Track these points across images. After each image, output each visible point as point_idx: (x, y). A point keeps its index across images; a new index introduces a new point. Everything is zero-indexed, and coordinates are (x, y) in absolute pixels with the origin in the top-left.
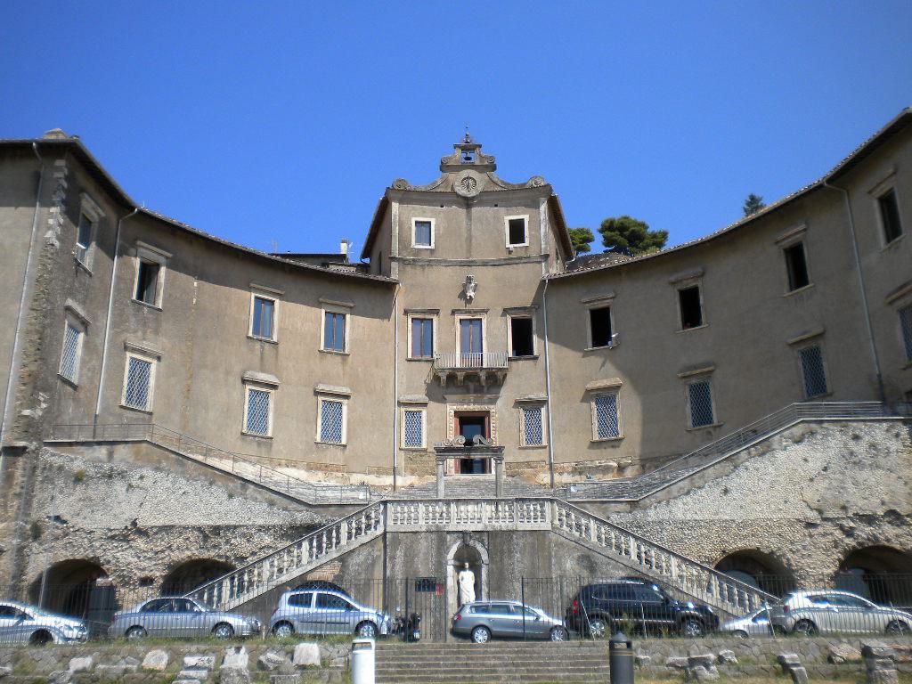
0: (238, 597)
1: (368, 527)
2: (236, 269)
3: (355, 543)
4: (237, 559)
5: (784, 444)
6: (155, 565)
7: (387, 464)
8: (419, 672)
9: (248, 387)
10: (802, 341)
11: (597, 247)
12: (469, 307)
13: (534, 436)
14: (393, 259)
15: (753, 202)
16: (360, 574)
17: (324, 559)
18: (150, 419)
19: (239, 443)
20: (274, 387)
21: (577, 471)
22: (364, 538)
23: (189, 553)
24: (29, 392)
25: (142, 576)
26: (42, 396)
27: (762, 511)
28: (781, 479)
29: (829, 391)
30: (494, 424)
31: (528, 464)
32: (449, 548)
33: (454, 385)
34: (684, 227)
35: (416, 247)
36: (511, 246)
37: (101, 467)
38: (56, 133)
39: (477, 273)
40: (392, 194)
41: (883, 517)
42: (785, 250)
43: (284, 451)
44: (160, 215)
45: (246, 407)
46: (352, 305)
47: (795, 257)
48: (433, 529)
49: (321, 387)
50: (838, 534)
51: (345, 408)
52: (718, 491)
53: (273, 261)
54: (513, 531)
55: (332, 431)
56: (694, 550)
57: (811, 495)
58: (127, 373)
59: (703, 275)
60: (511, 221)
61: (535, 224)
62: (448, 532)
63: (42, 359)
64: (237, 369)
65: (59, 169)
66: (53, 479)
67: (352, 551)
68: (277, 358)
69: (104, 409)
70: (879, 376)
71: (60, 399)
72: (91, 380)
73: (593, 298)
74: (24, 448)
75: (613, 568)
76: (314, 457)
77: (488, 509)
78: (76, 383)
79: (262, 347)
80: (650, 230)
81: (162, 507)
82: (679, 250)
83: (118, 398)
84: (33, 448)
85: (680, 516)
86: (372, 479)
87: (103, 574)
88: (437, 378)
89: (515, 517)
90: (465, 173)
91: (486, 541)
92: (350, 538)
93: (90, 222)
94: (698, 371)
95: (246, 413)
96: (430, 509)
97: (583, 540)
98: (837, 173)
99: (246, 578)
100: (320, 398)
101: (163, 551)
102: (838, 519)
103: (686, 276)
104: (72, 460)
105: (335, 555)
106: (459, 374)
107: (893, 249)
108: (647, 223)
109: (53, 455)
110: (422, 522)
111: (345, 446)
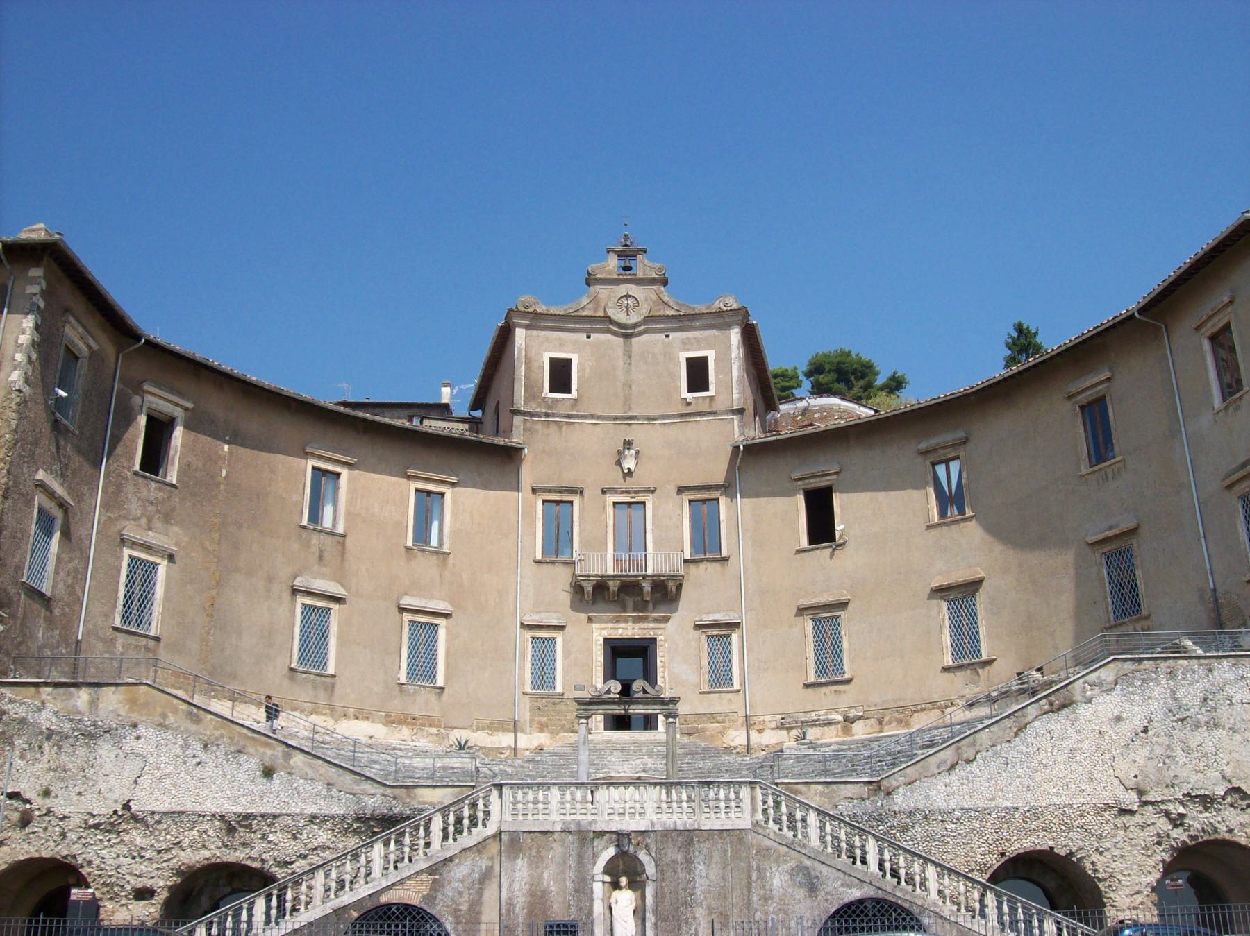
1: (474, 822)
2: (286, 427)
3: (453, 848)
4: (278, 864)
5: (1089, 693)
6: (158, 869)
7: (502, 716)
9: (301, 600)
12: (631, 483)
13: (720, 677)
15: (1023, 341)
16: (461, 894)
17: (406, 870)
19: (286, 682)
20: (338, 600)
22: (466, 840)
23: (207, 854)
25: (140, 886)
27: (1058, 794)
28: (1085, 745)
29: (1144, 613)
30: (662, 657)
31: (712, 717)
32: (596, 856)
33: (604, 599)
36: (690, 396)
37: (80, 721)
38: (35, 232)
39: (638, 433)
41: (1223, 798)
44: (178, 347)
45: (297, 630)
47: (1095, 413)
48: (573, 827)
49: (407, 601)
50: (1163, 825)
51: (442, 633)
55: (422, 666)
56: (961, 852)
57: (1127, 769)
58: (123, 578)
59: (965, 441)
60: (689, 360)
61: (724, 358)
64: (284, 573)
65: (33, 281)
66: (12, 737)
67: (451, 859)
69: (87, 633)
70: (1214, 590)
72: (71, 589)
76: (396, 705)
81: (167, 783)
82: (990, 386)
83: (108, 615)
85: (940, 803)
86: (479, 738)
87: (83, 883)
89: (697, 810)
90: (623, 289)
91: (653, 847)
92: (445, 838)
93: (77, 358)
96: (568, 797)
98: (1166, 289)
99: (289, 896)
100: (407, 617)
101: (168, 850)
105: (423, 865)
106: (611, 583)
107: (1231, 409)
109: (11, 701)
111: (442, 689)
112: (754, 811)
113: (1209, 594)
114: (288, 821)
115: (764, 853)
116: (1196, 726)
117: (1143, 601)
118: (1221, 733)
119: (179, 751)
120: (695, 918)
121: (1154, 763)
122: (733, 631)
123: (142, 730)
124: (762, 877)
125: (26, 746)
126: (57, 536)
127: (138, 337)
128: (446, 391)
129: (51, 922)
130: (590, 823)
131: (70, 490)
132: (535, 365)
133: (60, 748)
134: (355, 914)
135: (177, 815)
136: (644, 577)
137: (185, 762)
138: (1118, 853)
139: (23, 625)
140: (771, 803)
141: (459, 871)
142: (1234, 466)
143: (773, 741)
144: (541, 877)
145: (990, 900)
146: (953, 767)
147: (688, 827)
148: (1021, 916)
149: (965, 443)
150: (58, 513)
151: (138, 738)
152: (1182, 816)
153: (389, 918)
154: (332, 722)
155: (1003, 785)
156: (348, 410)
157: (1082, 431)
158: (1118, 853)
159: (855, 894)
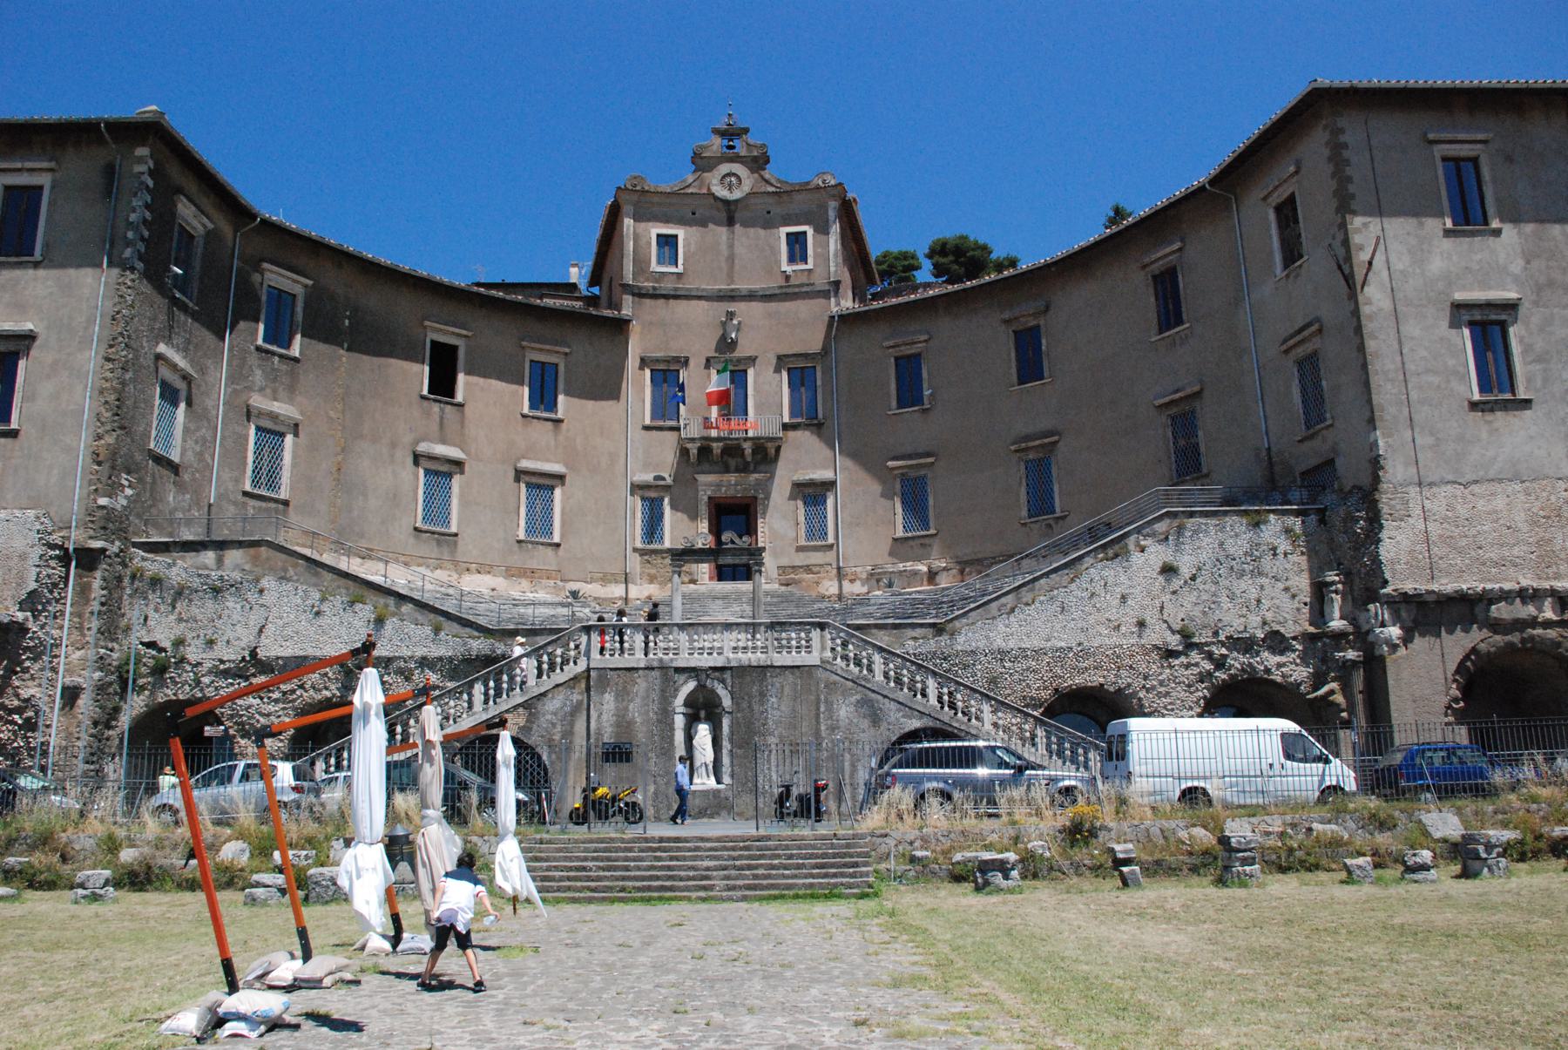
1: (565, 662)
3: (547, 683)
7: (616, 568)
8: (599, 879)
10: (1172, 402)
11: (924, 274)
14: (627, 288)
15: (1119, 213)
16: (554, 725)
18: (285, 513)
19: (412, 540)
21: (875, 578)
22: (559, 677)
23: (327, 693)
24: (106, 474)
26: (124, 479)
29: (1205, 471)
31: (808, 569)
32: (677, 690)
34: (1030, 242)
40: (624, 197)
41: (1263, 640)
42: (1155, 277)
47: (1167, 285)
48: (655, 664)
49: (525, 464)
52: (1056, 607)
55: (540, 522)
59: (1047, 308)
63: (122, 428)
64: (407, 439)
65: (141, 160)
67: (544, 694)
69: (219, 497)
70: (1269, 449)
71: (154, 482)
73: (899, 341)
74: (103, 550)
76: (517, 559)
77: (742, 638)
79: (442, 410)
80: (994, 256)
81: (289, 631)
83: (238, 480)
84: (115, 549)
85: (999, 643)
88: (684, 452)
90: (725, 168)
91: (729, 681)
93: (192, 237)
94: (1037, 442)
97: (865, 679)
102: (1207, 644)
103: (1025, 311)
105: (520, 700)
106: (714, 445)
109: (144, 559)
111: (558, 545)
112: (823, 648)
116: (1242, 574)
117: (1203, 460)
121: (1201, 608)
123: (264, 583)
124: (830, 709)
126: (183, 406)
127: (253, 216)
128: (574, 271)
131: (192, 362)
132: (643, 242)
136: (746, 439)
138: (1162, 689)
139: (152, 490)
141: (553, 705)
142: (1291, 331)
144: (626, 709)
145: (1040, 732)
146: (1012, 610)
150: (180, 385)
152: (1224, 657)
154: (456, 576)
155: (1058, 627)
157: (1153, 299)
158: (1162, 689)
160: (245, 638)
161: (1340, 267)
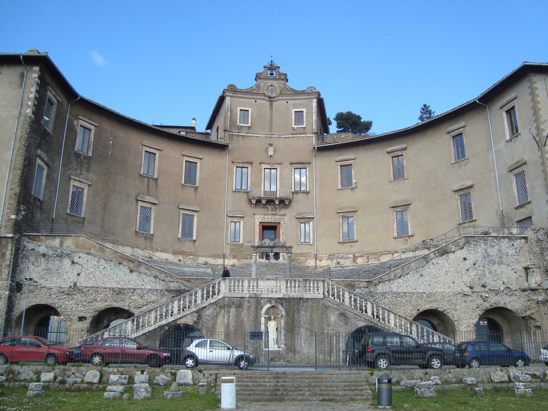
0: (137, 332)
3: (206, 304)
15: (426, 109)
17: (187, 312)
19: (134, 237)
20: (154, 204)
21: (330, 257)
22: (211, 300)
23: (107, 303)
28: (452, 269)
30: (282, 231)
32: (262, 308)
35: (240, 125)
36: (296, 127)
43: (160, 243)
45: (138, 216)
46: (201, 157)
48: (253, 296)
50: (480, 301)
53: (155, 129)
54: (301, 299)
55: (187, 232)
57: (466, 279)
61: (309, 112)
62: (262, 298)
64: (134, 193)
66: (28, 256)
67: (205, 307)
68: (157, 188)
75: (358, 321)
78: (42, 199)
79: (148, 181)
80: (362, 120)
83: (65, 209)
85: (395, 290)
86: (211, 261)
90: (270, 82)
92: (203, 299)
95: (138, 220)
99: (141, 320)
100: (182, 212)
104: (39, 246)
105: (194, 310)
106: (263, 201)
108: (361, 116)
110: (246, 292)
111: (195, 241)
113: (500, 213)
114: (139, 291)
115: (327, 307)
116: (494, 263)
117: (474, 214)
118: (503, 266)
119: (96, 263)
120: (300, 332)
122: (311, 221)
124: (327, 317)
125: (35, 260)
129: (41, 328)
130: (260, 294)
133: (48, 261)
134: (167, 328)
135: (96, 289)
137: (98, 268)
140: (330, 288)
141: (209, 312)
143: (325, 265)
145: (414, 328)
147: (298, 297)
148: (425, 334)
149: (405, 149)
151: (80, 257)
153: (181, 330)
156: (159, 128)
157: (453, 147)
159: (362, 324)
160: (73, 278)
161: (534, 138)
